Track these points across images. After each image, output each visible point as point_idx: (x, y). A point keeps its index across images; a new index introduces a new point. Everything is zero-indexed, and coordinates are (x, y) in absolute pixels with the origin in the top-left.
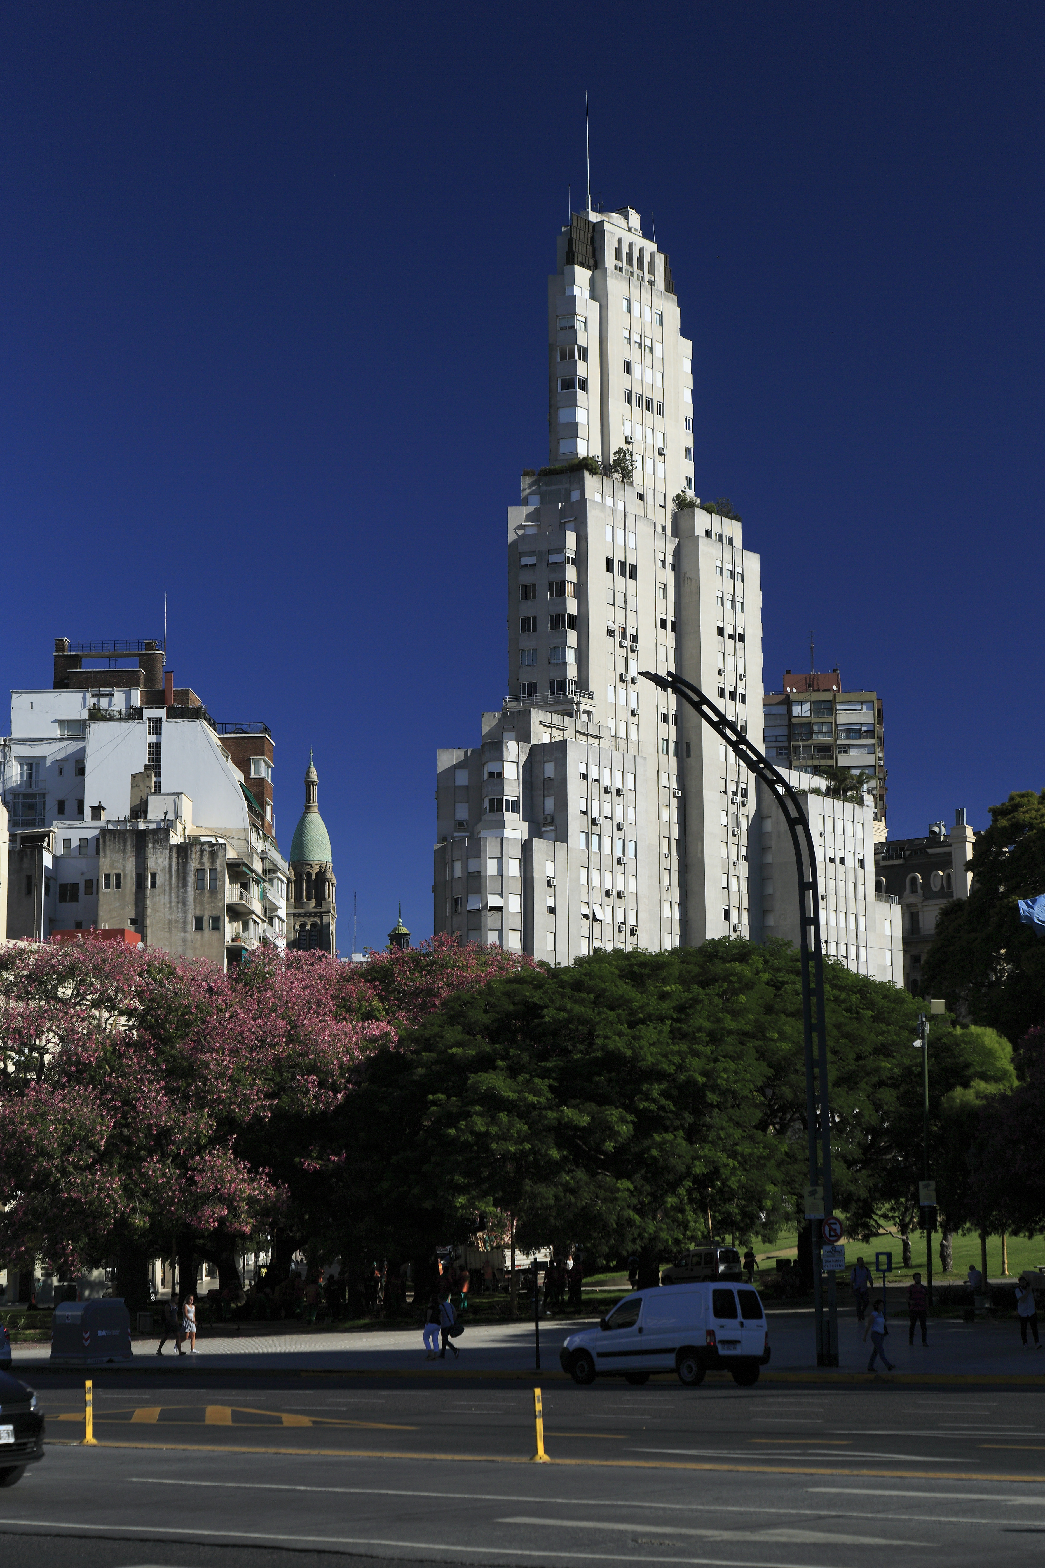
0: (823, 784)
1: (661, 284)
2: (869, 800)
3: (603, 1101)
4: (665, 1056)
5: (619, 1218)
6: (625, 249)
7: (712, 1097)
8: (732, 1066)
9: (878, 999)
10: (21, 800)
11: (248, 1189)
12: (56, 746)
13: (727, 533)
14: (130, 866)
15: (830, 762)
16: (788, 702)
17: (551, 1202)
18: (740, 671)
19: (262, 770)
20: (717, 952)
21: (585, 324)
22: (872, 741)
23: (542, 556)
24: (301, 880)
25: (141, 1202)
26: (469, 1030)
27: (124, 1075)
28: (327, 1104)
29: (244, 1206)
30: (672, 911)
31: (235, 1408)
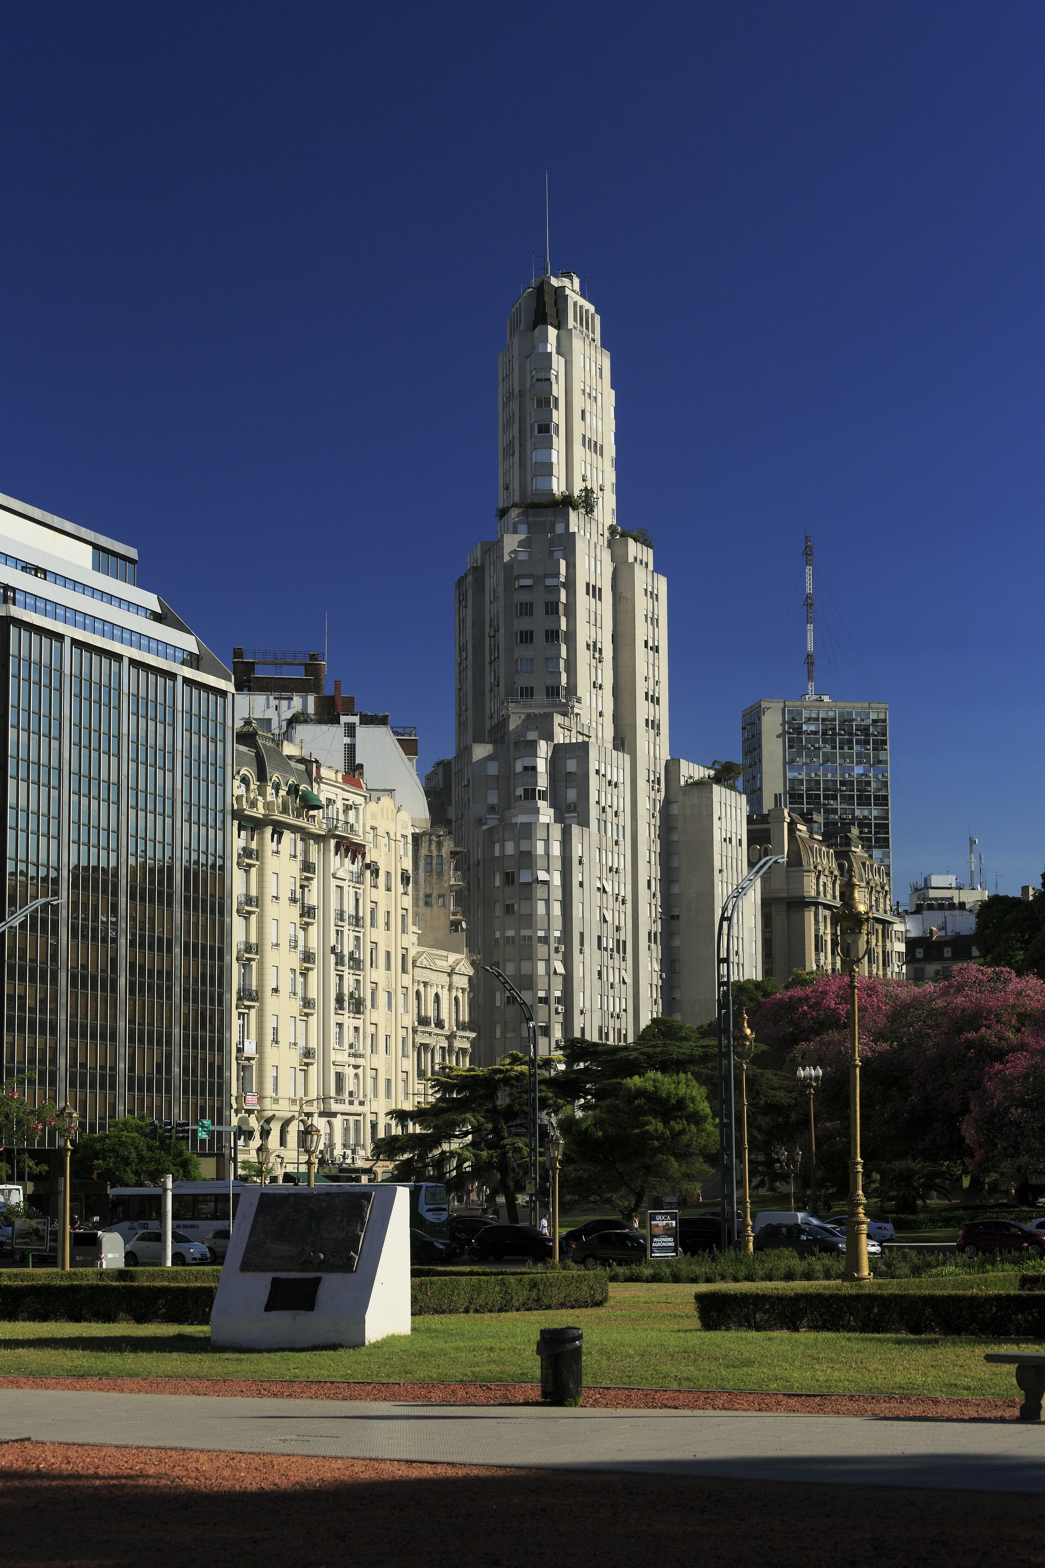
1: (598, 342)
23: (538, 579)
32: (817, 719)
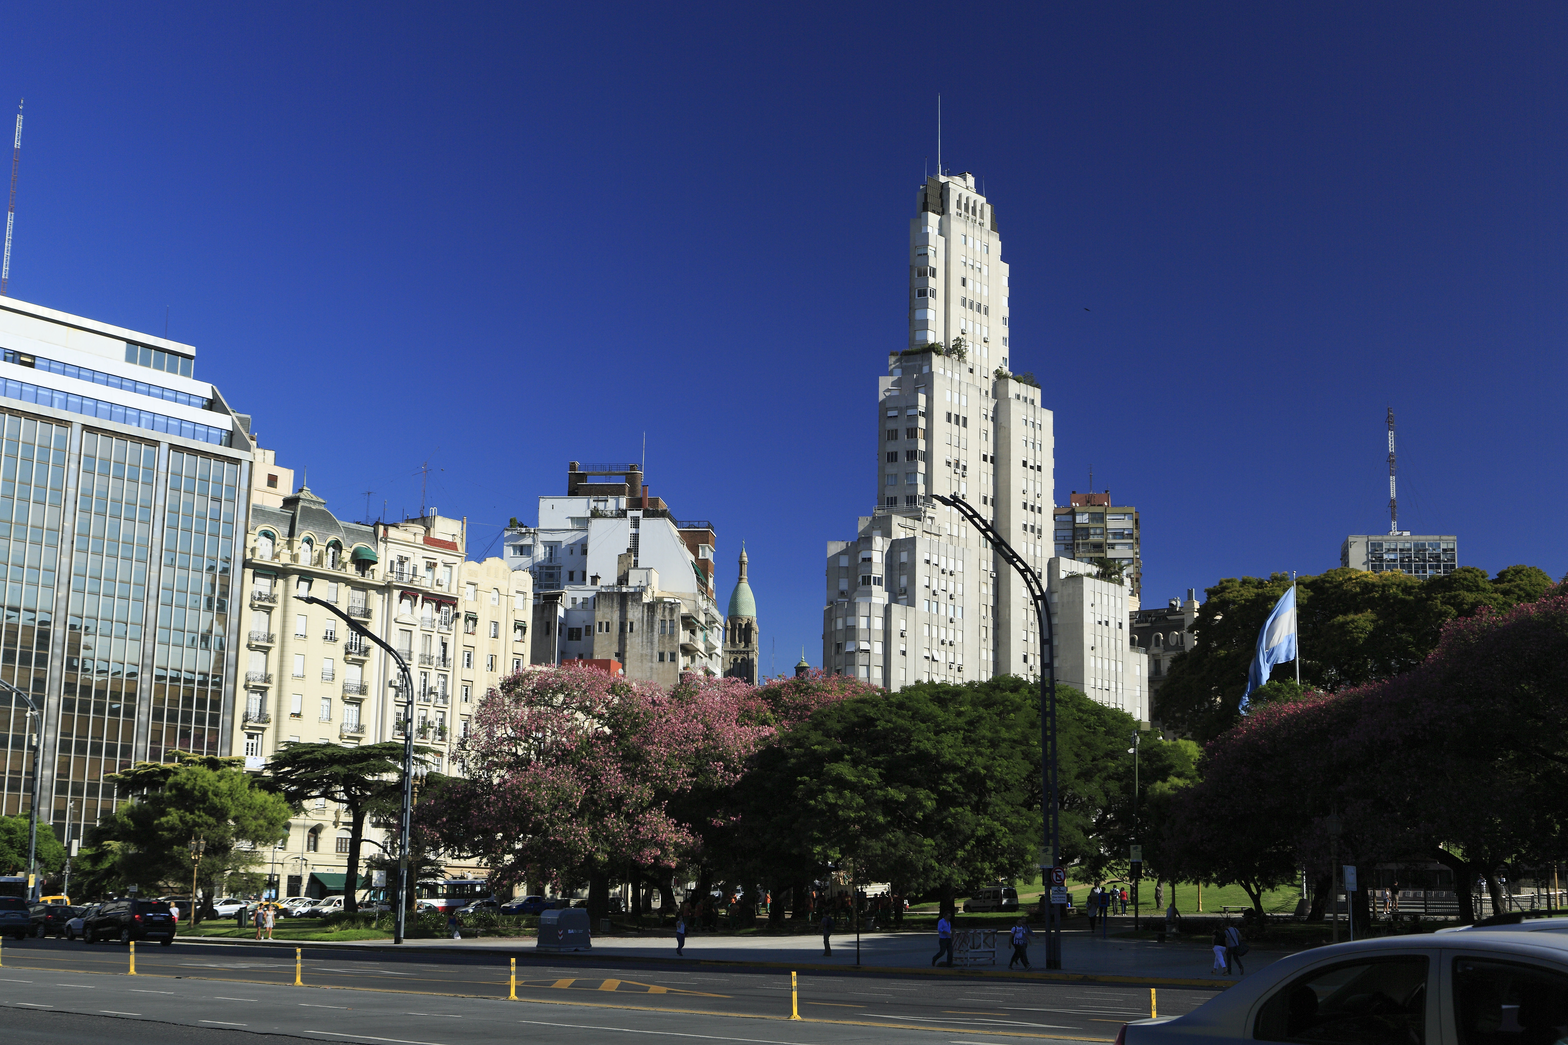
0: (1094, 570)
2: (1127, 581)
3: (916, 784)
4: (959, 755)
5: (924, 864)
6: (964, 201)
7: (990, 784)
8: (1006, 763)
9: (1108, 719)
10: (545, 571)
11: (675, 838)
12: (569, 534)
13: (1030, 396)
14: (616, 617)
15: (1102, 555)
16: (1073, 513)
17: (879, 852)
18: (1038, 491)
19: (707, 553)
20: (999, 685)
21: (935, 252)
22: (1131, 541)
23: (902, 410)
24: (735, 628)
25: (602, 843)
26: (827, 734)
27: (594, 759)
28: (730, 782)
29: (672, 849)
30: (988, 656)
32: (1395, 550)
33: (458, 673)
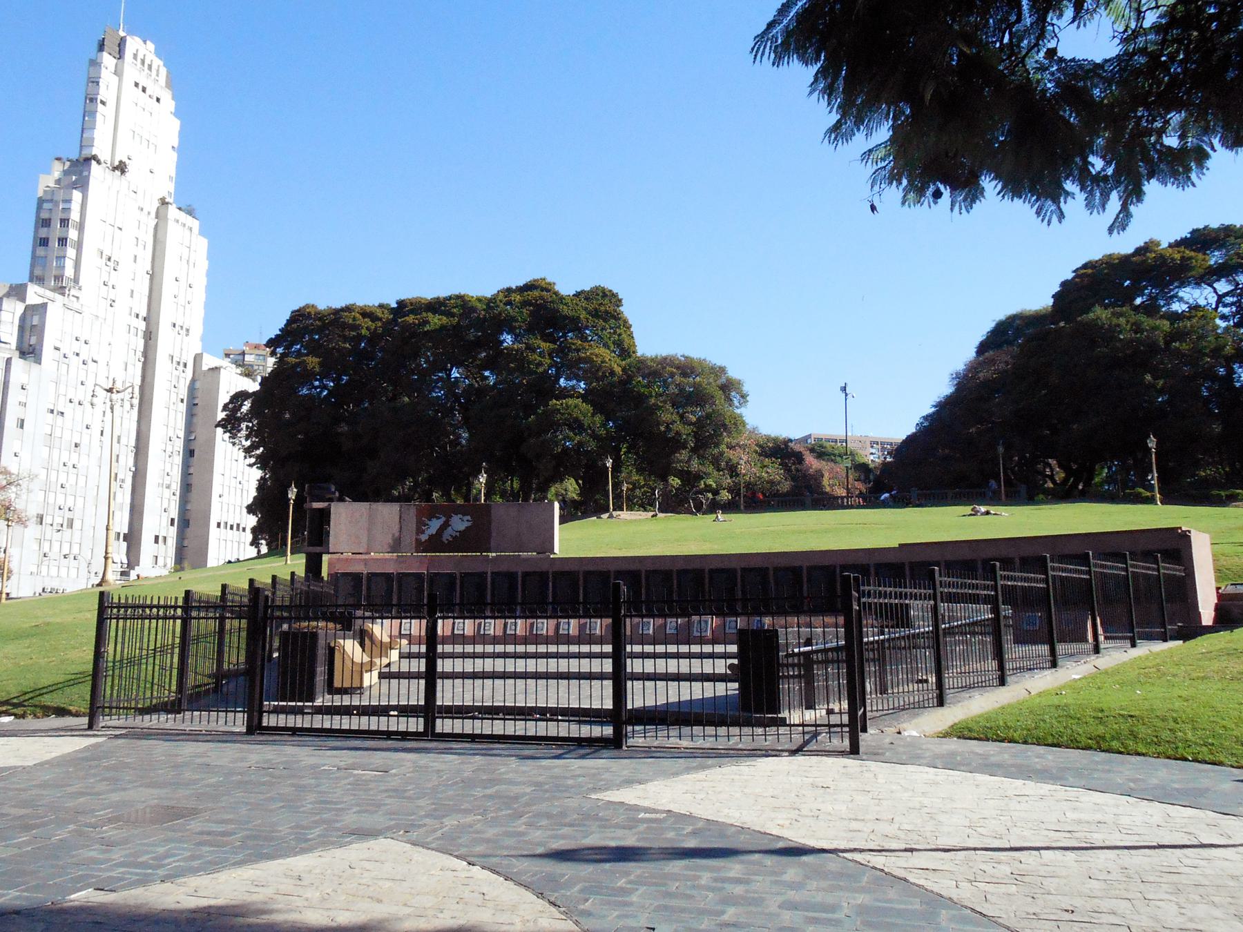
31: (1056, 641)
33: (902, 634)
